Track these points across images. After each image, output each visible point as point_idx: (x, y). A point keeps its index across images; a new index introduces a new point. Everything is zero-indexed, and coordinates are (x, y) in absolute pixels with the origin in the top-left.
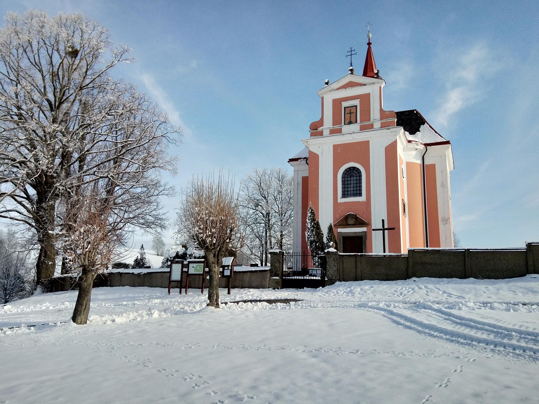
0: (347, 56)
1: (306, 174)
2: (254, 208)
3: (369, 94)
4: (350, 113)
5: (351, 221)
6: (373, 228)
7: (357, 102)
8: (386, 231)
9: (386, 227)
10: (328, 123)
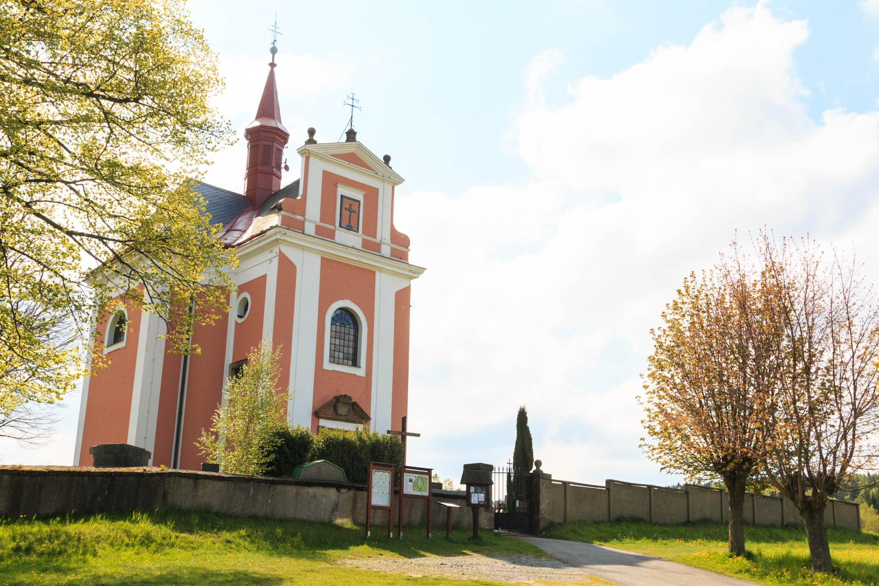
3: (324, 172)
5: (343, 410)
7: (359, 196)
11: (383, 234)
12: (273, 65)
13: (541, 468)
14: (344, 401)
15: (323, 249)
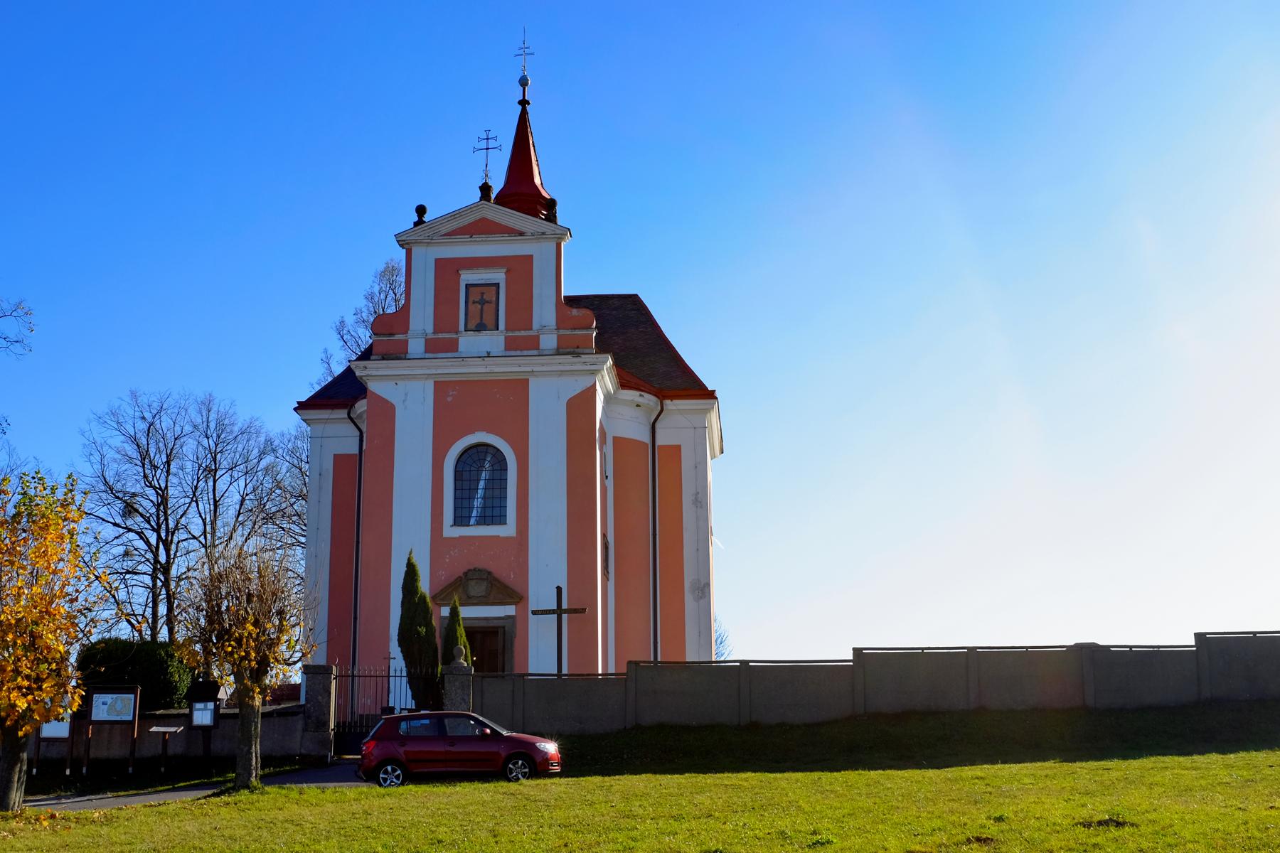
1: (350, 446)
2: (119, 520)
4: (483, 302)
6: (533, 606)
7: (498, 276)
8: (565, 617)
9: (565, 606)
10: (422, 320)
12: (524, 103)
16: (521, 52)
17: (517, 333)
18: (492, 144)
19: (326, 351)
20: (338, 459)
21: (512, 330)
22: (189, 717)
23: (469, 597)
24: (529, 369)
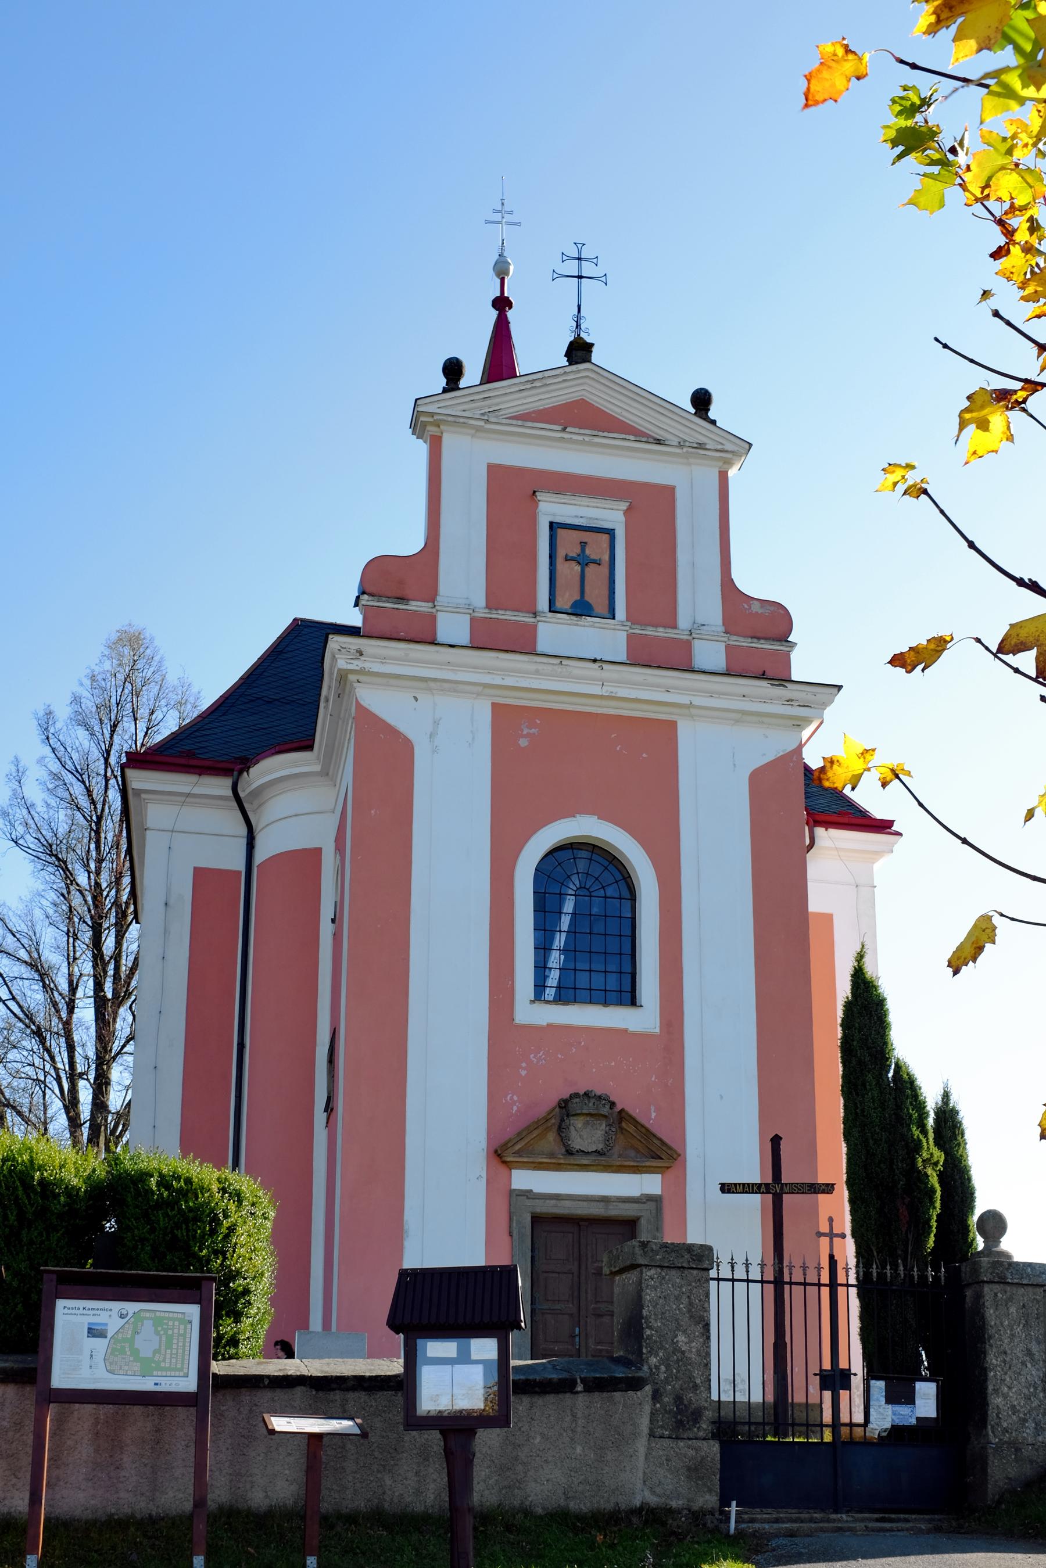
0: (556, 276)
7: (611, 515)
10: (463, 581)
11: (698, 605)
12: (502, 304)
13: (1007, 1244)
14: (590, 1107)
15: (487, 679)
16: (497, 217)
17: (650, 632)
18: (587, 269)
19: (17, 761)
20: (201, 875)
21: (644, 624)
22: (404, 1385)
23: (569, 1152)
24: (684, 700)
